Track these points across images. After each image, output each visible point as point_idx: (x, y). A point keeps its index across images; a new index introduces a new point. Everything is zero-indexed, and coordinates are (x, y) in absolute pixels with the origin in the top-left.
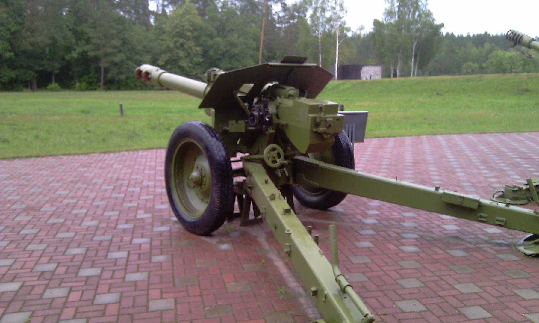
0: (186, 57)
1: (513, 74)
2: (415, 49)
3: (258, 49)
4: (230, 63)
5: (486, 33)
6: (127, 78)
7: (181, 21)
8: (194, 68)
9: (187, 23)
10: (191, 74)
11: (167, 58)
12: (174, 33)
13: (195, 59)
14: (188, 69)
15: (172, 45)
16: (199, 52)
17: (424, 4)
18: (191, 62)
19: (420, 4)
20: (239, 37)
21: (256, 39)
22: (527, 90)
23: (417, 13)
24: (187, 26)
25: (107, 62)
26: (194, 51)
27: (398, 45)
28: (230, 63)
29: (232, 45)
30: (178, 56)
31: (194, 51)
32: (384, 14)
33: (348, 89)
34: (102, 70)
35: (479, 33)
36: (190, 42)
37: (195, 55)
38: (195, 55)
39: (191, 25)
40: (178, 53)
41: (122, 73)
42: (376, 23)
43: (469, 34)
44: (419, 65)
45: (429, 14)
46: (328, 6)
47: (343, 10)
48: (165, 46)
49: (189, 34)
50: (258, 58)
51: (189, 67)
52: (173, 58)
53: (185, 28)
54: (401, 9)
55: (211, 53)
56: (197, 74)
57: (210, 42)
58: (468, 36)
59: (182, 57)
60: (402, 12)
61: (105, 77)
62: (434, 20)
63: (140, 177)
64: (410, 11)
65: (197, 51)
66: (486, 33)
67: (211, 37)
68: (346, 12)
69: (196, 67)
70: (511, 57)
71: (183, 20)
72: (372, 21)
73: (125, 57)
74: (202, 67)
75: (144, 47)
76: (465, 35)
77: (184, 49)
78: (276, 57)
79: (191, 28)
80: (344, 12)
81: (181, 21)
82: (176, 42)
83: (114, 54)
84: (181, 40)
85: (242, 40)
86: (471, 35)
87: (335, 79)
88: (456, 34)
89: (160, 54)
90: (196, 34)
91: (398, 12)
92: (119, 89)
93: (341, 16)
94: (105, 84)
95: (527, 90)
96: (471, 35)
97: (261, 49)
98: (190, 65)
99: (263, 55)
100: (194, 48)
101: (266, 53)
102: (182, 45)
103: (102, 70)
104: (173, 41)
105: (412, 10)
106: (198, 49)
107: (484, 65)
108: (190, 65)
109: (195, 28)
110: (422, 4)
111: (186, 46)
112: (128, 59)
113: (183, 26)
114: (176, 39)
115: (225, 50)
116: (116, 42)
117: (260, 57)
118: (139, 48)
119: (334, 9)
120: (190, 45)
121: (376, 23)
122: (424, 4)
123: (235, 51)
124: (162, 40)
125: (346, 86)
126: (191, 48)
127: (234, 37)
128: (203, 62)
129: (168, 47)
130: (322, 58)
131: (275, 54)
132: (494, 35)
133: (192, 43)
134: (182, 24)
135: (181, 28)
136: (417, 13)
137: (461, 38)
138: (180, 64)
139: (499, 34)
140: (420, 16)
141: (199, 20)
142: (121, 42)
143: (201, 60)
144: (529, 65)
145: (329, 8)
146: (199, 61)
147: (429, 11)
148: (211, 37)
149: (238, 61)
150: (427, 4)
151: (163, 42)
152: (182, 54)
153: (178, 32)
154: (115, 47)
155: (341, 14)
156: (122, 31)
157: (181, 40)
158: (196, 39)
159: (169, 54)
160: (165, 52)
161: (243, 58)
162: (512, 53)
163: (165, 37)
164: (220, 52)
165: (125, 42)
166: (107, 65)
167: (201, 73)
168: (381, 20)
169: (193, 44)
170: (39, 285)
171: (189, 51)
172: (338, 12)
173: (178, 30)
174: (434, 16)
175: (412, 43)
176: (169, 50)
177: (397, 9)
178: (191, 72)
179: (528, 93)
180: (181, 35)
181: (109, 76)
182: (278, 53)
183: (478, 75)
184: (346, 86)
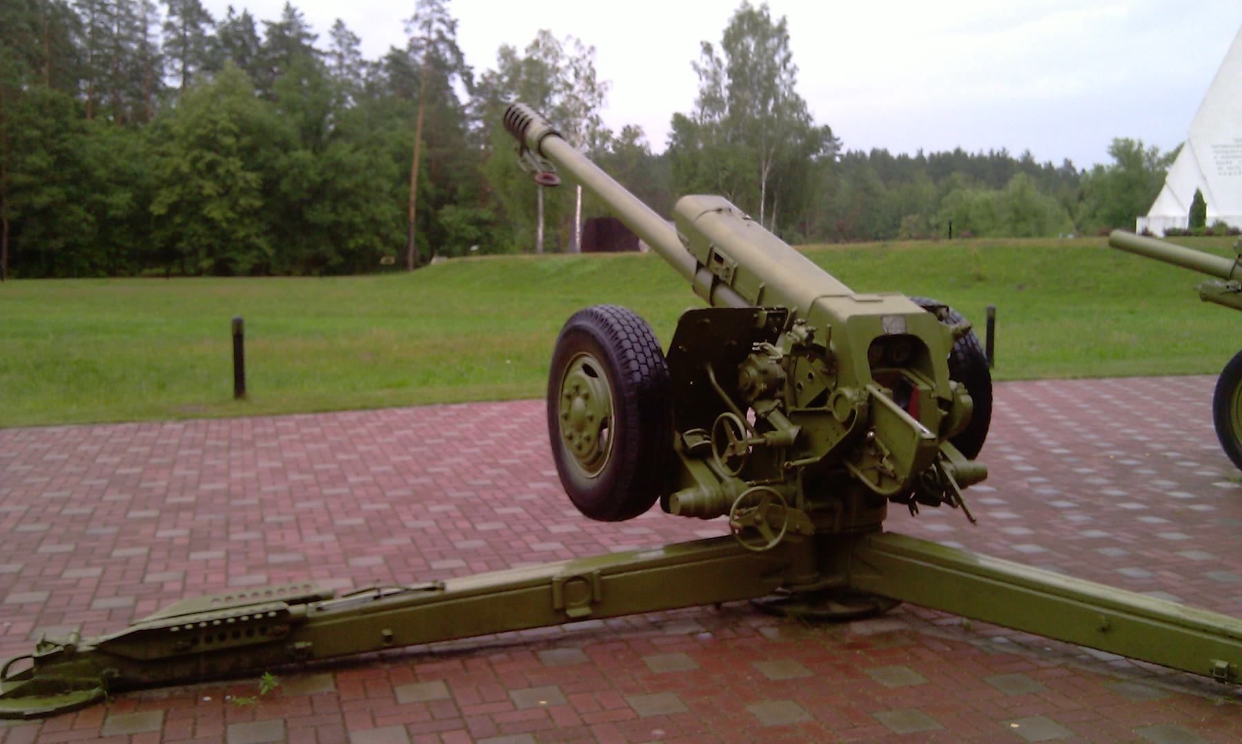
0: (220, 195)
1: (954, 240)
2: (767, 183)
3: (406, 177)
4: (334, 210)
5: (958, 151)
6: (68, 247)
7: (208, 110)
8: (242, 223)
9: (225, 115)
10: (234, 236)
11: (175, 198)
12: (191, 138)
13: (243, 202)
14: (224, 225)
15: (185, 168)
16: (254, 185)
17: (788, 82)
18: (232, 209)
19: (777, 81)
20: (356, 149)
21: (402, 156)
22: (980, 279)
23: (772, 103)
24: (224, 121)
25: (13, 208)
26: (241, 183)
27: (726, 173)
28: (334, 210)
29: (338, 166)
30: (200, 194)
31: (241, 183)
32: (697, 102)
33: (593, 273)
34: (6, 227)
35: (935, 152)
36: (231, 159)
37: (245, 192)
38: (245, 192)
39: (233, 121)
40: (201, 187)
41: (55, 236)
42: (679, 122)
43: (921, 152)
44: (778, 221)
45: (797, 104)
46: (558, 80)
47: (593, 90)
48: (168, 171)
49: (229, 141)
50: (408, 200)
51: (229, 221)
52: (189, 198)
53: (219, 127)
54: (738, 93)
55: (285, 186)
56: (247, 236)
57: (282, 161)
58: (920, 157)
59: (209, 197)
60: (738, 100)
61: (12, 246)
62: (809, 118)
63: (250, 474)
64: (755, 97)
65: (246, 182)
66: (958, 151)
67: (286, 147)
68: (601, 96)
69: (247, 221)
70: (987, 204)
71: (214, 107)
72: (670, 118)
73: (63, 196)
74: (260, 220)
75: (118, 171)
76: (913, 155)
77: (217, 177)
78: (455, 197)
79: (235, 128)
80: (595, 95)
81: (208, 110)
82: (195, 161)
83: (30, 188)
84: (210, 156)
85: (362, 157)
86: (926, 154)
87: (573, 251)
88: (894, 153)
89: (159, 188)
90: (246, 141)
91: (730, 98)
92: (49, 274)
93: (590, 104)
94: (12, 263)
95: (980, 279)
96: (926, 154)
97: (414, 180)
98: (230, 215)
99: (424, 194)
100: (240, 174)
101: (430, 187)
102: (211, 166)
103: (6, 227)
104: (189, 158)
105: (760, 95)
106: (251, 176)
107: (933, 221)
108: (230, 215)
109: (245, 127)
110: (783, 81)
111: (221, 171)
112: (71, 200)
113: (215, 123)
114: (196, 153)
115: (319, 179)
116: (38, 159)
117: (413, 198)
118: (102, 173)
119: (570, 87)
120: (232, 168)
121: (679, 122)
122: (788, 82)
123: (345, 183)
124: (163, 155)
125: (588, 268)
126: (233, 175)
127: (342, 151)
128: (264, 207)
129: (176, 170)
130: (544, 199)
131: (454, 190)
132: (976, 154)
133: (235, 163)
134: (213, 117)
135: (210, 126)
136: (772, 103)
137: (904, 159)
138: (205, 211)
139: (986, 153)
140: (777, 108)
141: (258, 110)
142: (51, 159)
143: (258, 203)
144: (1024, 219)
145: (558, 87)
146: (251, 206)
147: (797, 97)
148: (286, 147)
149: (356, 207)
150: (794, 83)
151: (164, 160)
152: (209, 188)
153: (201, 137)
154: (37, 172)
155: (586, 99)
156: (59, 132)
157: (210, 156)
158: (248, 153)
159: (178, 189)
160: (169, 183)
161: (367, 201)
162: (983, 195)
163: (171, 147)
164: (305, 185)
165: (63, 159)
166: (14, 215)
167: (258, 236)
168: (689, 116)
169: (239, 164)
170: (481, 648)
171: (229, 182)
172: (581, 96)
173: (200, 131)
174: (810, 109)
175: (760, 172)
176: (179, 178)
177: (726, 93)
178: (234, 232)
179: (981, 284)
180: (208, 143)
181: (23, 241)
182: (461, 189)
183: (878, 244)
184: (588, 268)
